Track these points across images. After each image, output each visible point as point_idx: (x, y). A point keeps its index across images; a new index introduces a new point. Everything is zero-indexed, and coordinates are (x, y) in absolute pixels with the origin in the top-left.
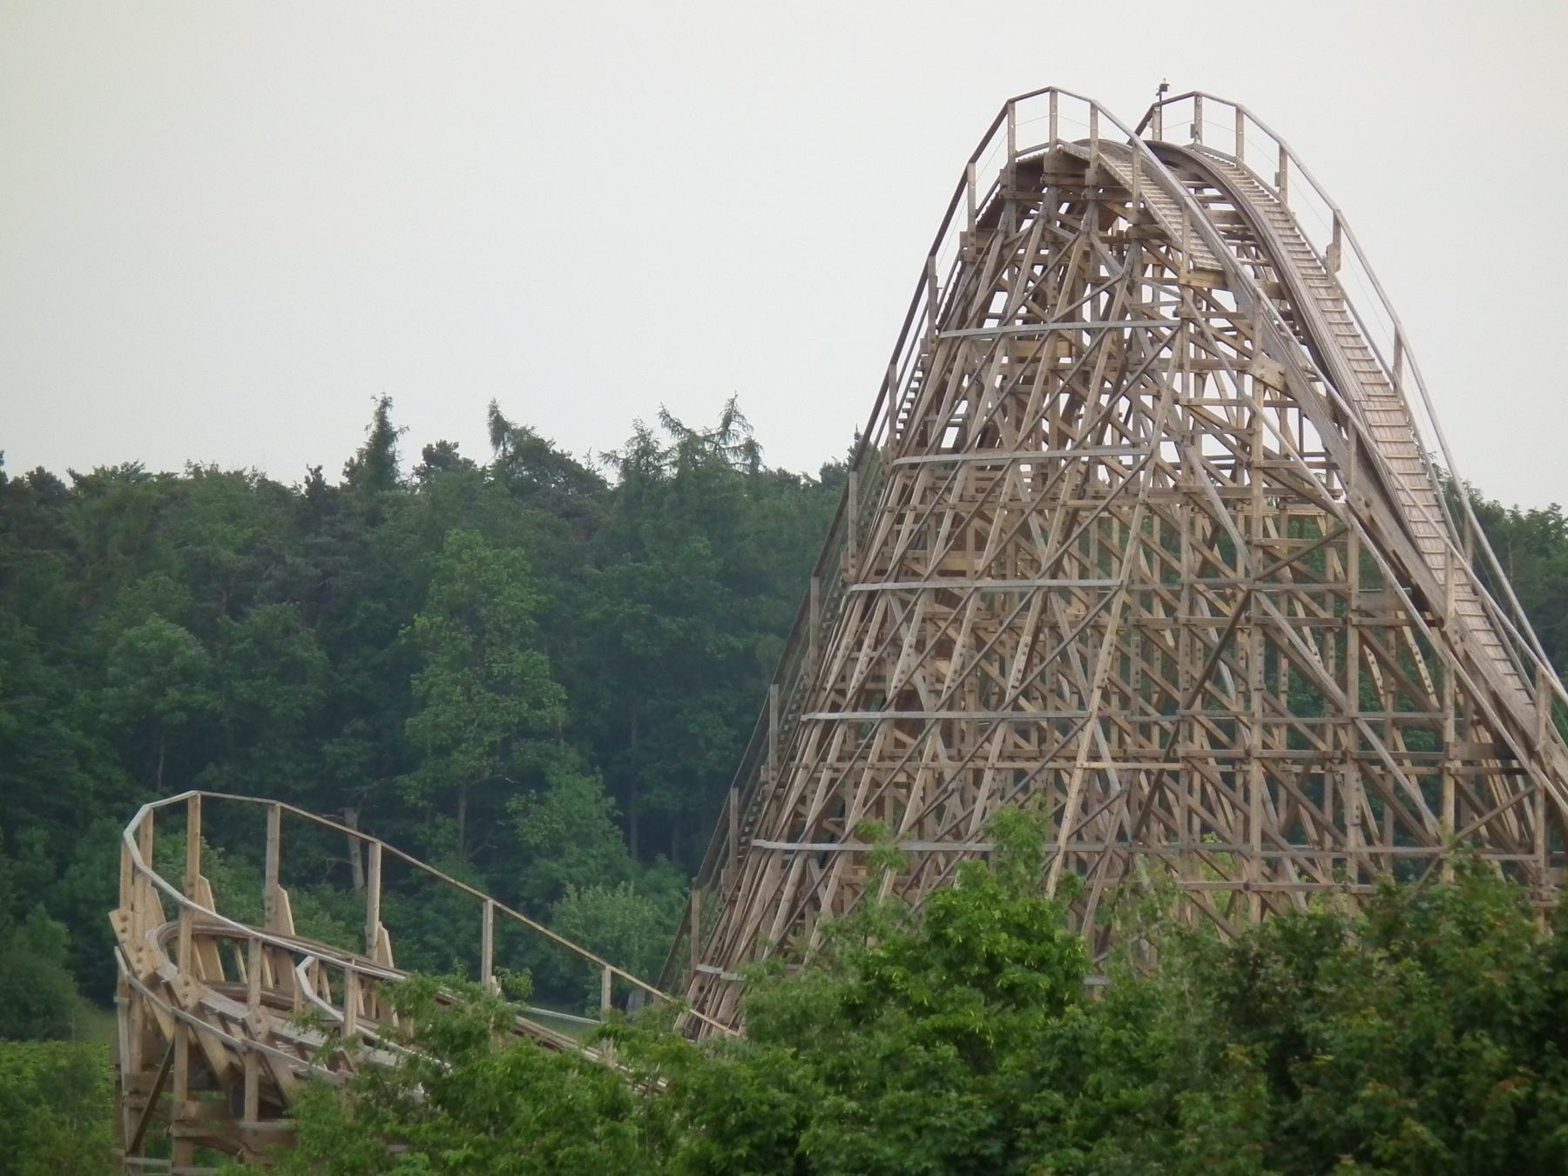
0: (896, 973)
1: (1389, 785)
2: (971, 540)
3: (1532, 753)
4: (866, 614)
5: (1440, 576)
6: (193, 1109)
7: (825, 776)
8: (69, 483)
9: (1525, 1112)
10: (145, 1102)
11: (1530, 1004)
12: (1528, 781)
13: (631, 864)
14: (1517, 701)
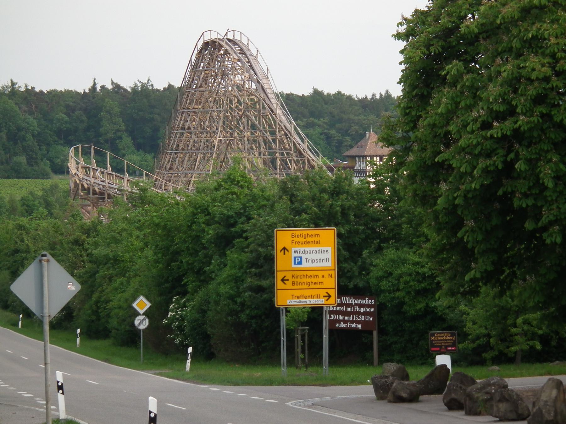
0: (223, 183)
1: (267, 140)
2: (198, 103)
3: (291, 135)
4: (182, 115)
5: (275, 107)
6: (82, 194)
7: (176, 141)
8: (46, 92)
9: (331, 206)
10: (74, 193)
11: (331, 189)
12: (290, 139)
13: (136, 151)
14: (288, 126)
